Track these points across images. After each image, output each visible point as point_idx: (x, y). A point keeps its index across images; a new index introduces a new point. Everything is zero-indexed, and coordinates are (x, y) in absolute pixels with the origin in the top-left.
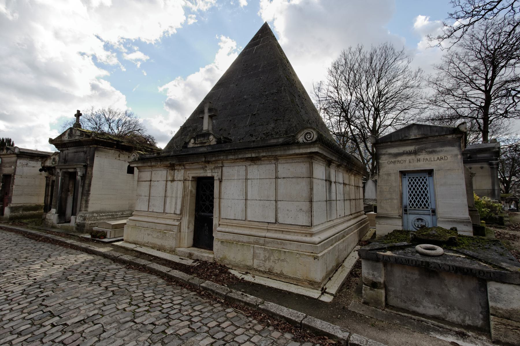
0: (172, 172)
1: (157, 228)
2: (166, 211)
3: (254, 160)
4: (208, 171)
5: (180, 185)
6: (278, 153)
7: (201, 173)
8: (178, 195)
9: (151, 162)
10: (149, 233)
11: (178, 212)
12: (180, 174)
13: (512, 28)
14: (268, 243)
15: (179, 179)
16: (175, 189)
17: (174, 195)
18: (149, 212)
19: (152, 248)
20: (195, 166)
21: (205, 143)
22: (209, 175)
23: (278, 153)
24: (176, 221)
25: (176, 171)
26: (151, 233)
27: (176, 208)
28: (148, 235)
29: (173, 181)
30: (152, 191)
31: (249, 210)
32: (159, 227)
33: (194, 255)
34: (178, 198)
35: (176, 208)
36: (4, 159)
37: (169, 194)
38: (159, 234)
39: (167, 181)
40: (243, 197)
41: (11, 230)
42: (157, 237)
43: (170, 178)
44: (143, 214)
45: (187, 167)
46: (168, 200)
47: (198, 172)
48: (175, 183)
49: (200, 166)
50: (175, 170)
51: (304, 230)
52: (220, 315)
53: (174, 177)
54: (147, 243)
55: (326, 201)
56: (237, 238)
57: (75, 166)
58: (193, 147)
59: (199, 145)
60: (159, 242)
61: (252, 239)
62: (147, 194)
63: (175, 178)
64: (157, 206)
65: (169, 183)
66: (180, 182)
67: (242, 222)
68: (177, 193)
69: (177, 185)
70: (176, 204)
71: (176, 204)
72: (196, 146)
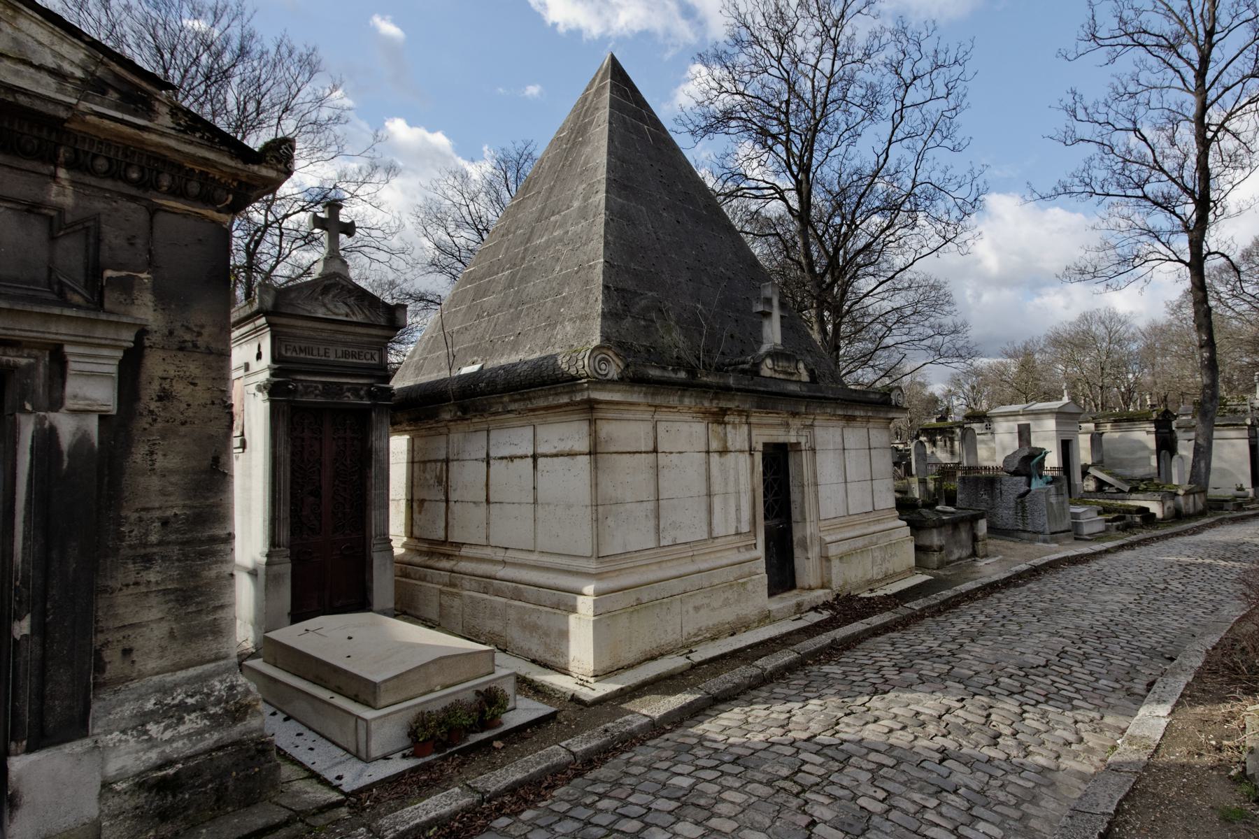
0: (720, 429)
2: (715, 535)
6: (857, 413)
7: (779, 436)
8: (742, 487)
10: (698, 603)
11: (745, 528)
12: (737, 436)
17: (731, 489)
18: (661, 550)
20: (772, 419)
22: (793, 440)
25: (729, 428)
26: (706, 601)
27: (738, 520)
28: (697, 609)
29: (724, 452)
34: (742, 495)
35: (738, 520)
37: (717, 487)
38: (728, 594)
39: (708, 452)
40: (841, 480)
41: (1178, 534)
42: (726, 603)
43: (715, 445)
46: (717, 502)
48: (730, 457)
49: (779, 421)
51: (867, 518)
53: (726, 442)
54: (696, 635)
55: (708, 452)
57: (56, 332)
60: (728, 615)
62: (647, 492)
63: (729, 444)
65: (715, 458)
66: (741, 456)
69: (737, 463)
70: (738, 509)
71: (738, 509)
72: (777, 376)
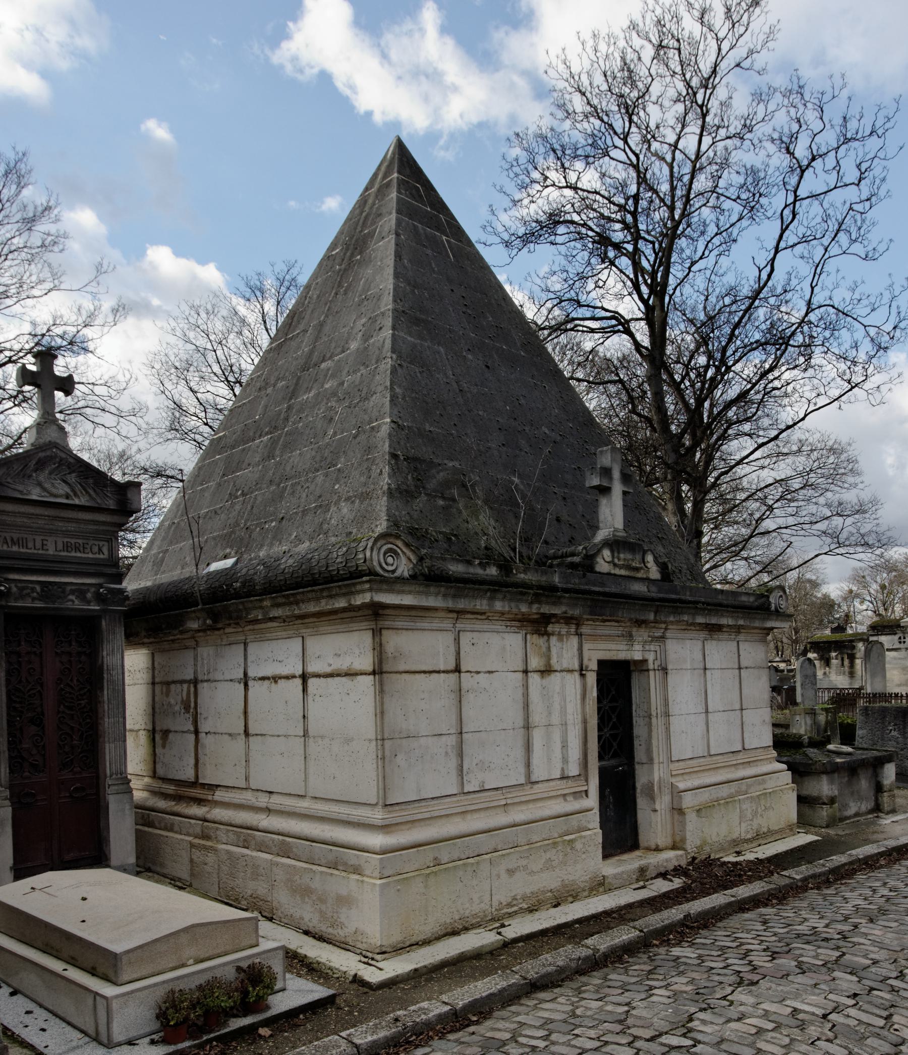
0: (541, 641)
1: (535, 838)
2: (534, 778)
3: (713, 630)
4: (637, 647)
5: (573, 683)
6: (724, 621)
7: (618, 651)
9: (492, 599)
12: (565, 651)
13: (829, 514)
14: (749, 786)
15: (565, 665)
16: (557, 699)
17: (556, 719)
18: (469, 797)
19: (531, 910)
20: (610, 629)
21: (637, 569)
22: (638, 656)
23: (724, 621)
24: (570, 798)
25: (554, 640)
26: (524, 862)
27: (565, 760)
28: (511, 872)
29: (547, 671)
30: (467, 712)
31: (711, 733)
32: (537, 833)
33: (651, 868)
34: (570, 727)
35: (565, 760)
36: (646, 590)
37: (537, 717)
42: (548, 866)
43: (535, 662)
44: (438, 808)
45: (585, 630)
47: (613, 646)
50: (548, 635)
52: (581, 1019)
53: (549, 658)
54: (509, 905)
56: (715, 793)
58: (609, 574)
59: (623, 572)
60: (550, 881)
61: (724, 791)
62: (448, 724)
64: (498, 764)
65: (534, 678)
66: (568, 676)
67: (702, 760)
68: (563, 711)
69: (563, 687)
70: (565, 746)
71: (565, 746)
72: (617, 571)
